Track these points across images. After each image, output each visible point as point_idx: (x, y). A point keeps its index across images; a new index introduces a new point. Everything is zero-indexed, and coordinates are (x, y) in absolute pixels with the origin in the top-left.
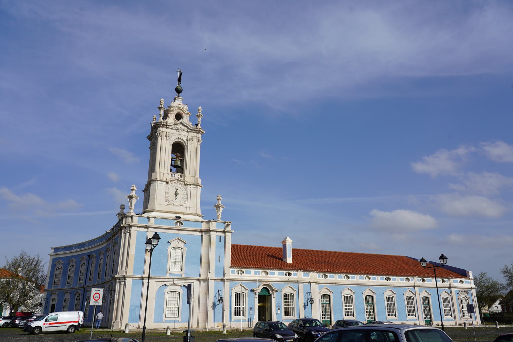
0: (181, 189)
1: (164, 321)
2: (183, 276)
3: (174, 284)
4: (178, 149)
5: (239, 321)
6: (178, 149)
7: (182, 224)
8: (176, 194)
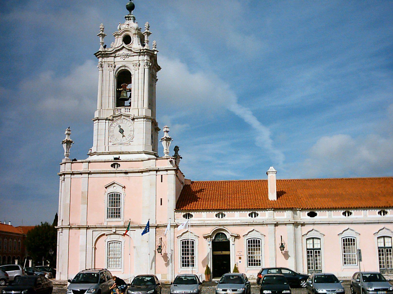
3: (115, 233)
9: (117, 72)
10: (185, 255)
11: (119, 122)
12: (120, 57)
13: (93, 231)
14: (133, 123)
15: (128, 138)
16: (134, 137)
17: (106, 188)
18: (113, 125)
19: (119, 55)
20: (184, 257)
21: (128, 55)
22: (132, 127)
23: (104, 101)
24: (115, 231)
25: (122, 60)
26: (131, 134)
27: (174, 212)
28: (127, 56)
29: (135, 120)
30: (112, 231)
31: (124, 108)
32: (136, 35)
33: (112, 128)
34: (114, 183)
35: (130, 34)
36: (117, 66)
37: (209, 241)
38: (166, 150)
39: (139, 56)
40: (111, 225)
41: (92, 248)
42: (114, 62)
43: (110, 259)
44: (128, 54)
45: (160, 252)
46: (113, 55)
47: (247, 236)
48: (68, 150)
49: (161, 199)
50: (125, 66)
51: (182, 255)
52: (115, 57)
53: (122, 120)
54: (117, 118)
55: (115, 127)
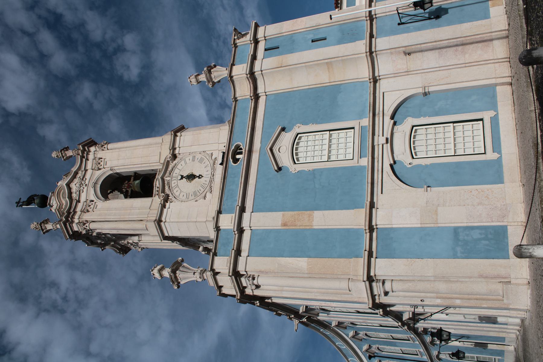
0: (183, 167)
1: (496, 156)
2: (366, 122)
3: (390, 141)
4: (117, 185)
5: (290, 69)
6: (117, 185)
7: (238, 147)
8: (191, 177)
17: (280, 169)
18: (177, 194)
28: (83, 179)
46: (74, 203)
49: (312, 41)
50: (96, 183)
53: (172, 178)
54: (167, 188)
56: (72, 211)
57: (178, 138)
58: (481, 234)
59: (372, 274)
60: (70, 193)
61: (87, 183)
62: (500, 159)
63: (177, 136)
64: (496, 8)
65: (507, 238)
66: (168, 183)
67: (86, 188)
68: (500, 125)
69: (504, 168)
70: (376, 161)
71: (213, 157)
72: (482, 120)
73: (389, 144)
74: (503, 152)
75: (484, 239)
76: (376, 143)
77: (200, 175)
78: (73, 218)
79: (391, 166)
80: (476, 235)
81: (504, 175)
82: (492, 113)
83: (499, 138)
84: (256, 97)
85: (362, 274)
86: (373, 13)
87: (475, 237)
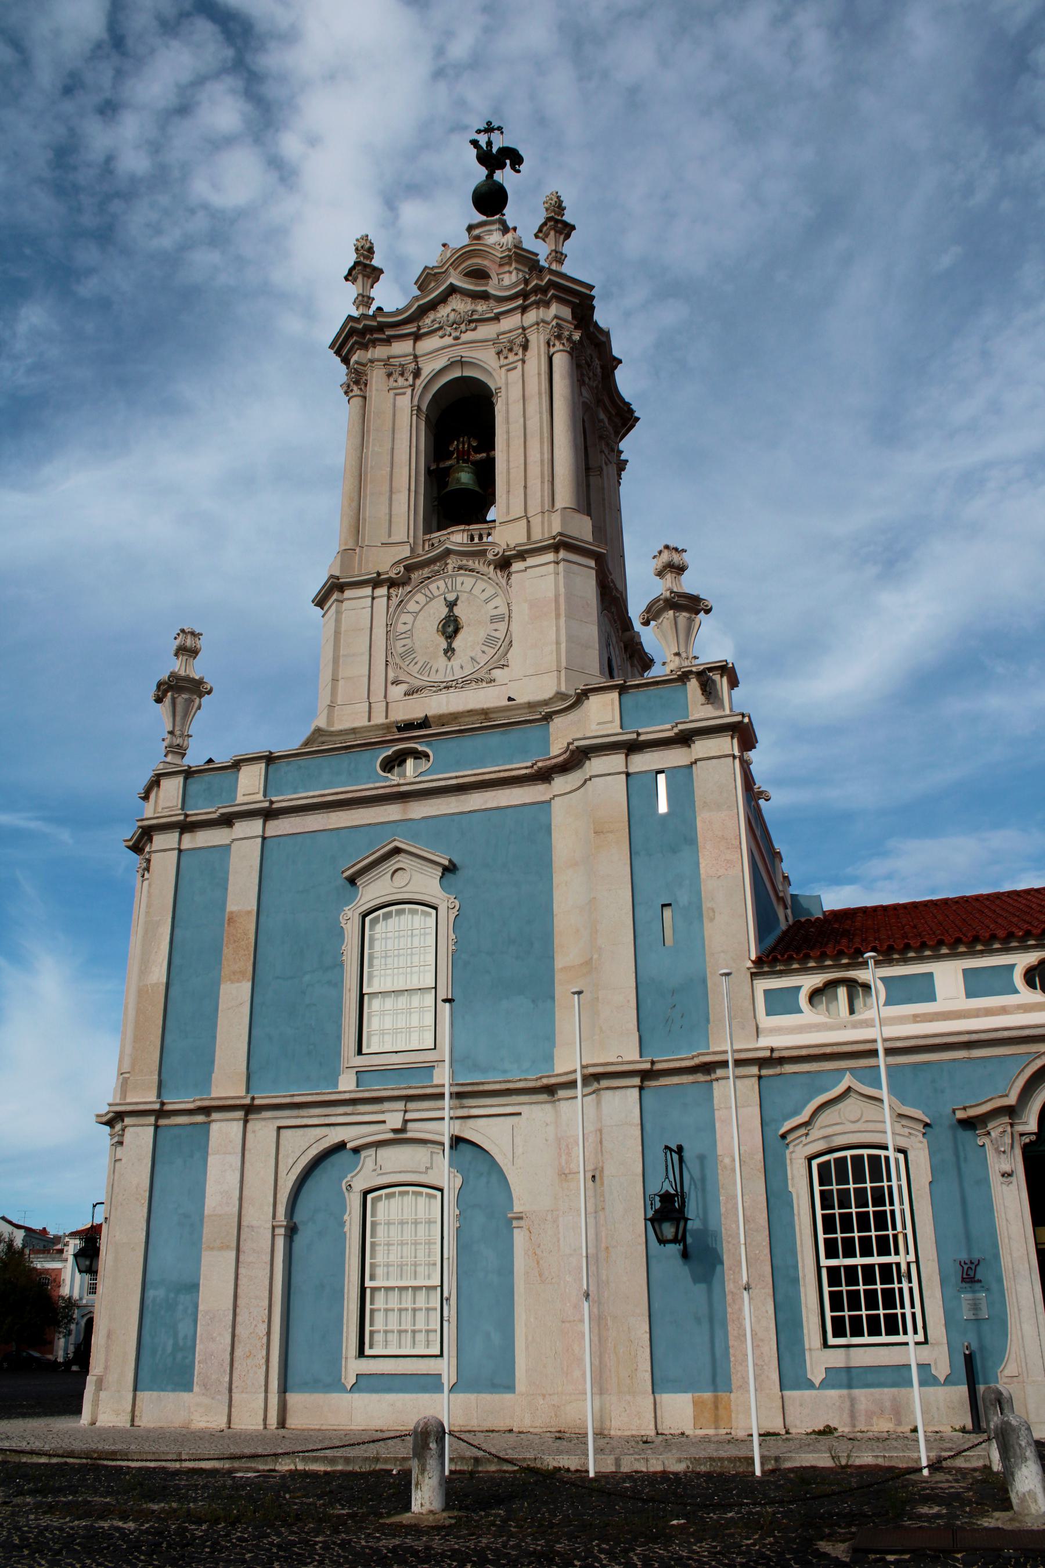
3: (400, 1138)
9: (429, 396)
10: (872, 1266)
11: (438, 586)
12: (440, 333)
13: (279, 1128)
14: (504, 582)
15: (483, 652)
16: (511, 643)
17: (352, 881)
18: (412, 606)
19: (437, 326)
20: (873, 1266)
21: (475, 317)
22: (498, 601)
23: (368, 512)
24: (399, 1126)
25: (448, 340)
26: (496, 634)
27: (752, 974)
28: (470, 322)
29: (516, 566)
30: (384, 1122)
31: (464, 530)
32: (511, 265)
33: (404, 618)
34: (397, 851)
35: (485, 266)
36: (428, 368)
37: (1008, 1149)
38: (678, 654)
39: (524, 309)
40: (483, 1083)
41: (274, 1228)
42: (416, 357)
43: (380, 1297)
44: (472, 315)
45: (675, 1241)
46: (411, 328)
47: (810, 1138)
48: (178, 718)
50: (461, 363)
51: (828, 1256)
52: (417, 337)
53: (451, 576)
54: (426, 572)
55: (417, 613)
56: (389, 332)
57: (550, 557)
58: (186, 1337)
59: (128, 1121)
60: (433, 306)
61: (465, 337)
62: (343, 1389)
63: (557, 551)
64: (690, 1410)
65: (174, 1390)
66: (436, 573)
67: (448, 340)
68: (420, 1395)
69: (321, 1395)
70: (348, 1109)
71: (497, 673)
72: (441, 1355)
73: (391, 1136)
74: (356, 1396)
75: (176, 1344)
76: (387, 1105)
77: (453, 650)
78: (374, 343)
79: (341, 1146)
80: (183, 1329)
81: (306, 1395)
82: (448, 1377)
83: (390, 1390)
84: (544, 776)
85: (128, 1100)
86: (720, 1073)
87: (180, 1326)
